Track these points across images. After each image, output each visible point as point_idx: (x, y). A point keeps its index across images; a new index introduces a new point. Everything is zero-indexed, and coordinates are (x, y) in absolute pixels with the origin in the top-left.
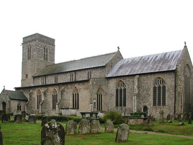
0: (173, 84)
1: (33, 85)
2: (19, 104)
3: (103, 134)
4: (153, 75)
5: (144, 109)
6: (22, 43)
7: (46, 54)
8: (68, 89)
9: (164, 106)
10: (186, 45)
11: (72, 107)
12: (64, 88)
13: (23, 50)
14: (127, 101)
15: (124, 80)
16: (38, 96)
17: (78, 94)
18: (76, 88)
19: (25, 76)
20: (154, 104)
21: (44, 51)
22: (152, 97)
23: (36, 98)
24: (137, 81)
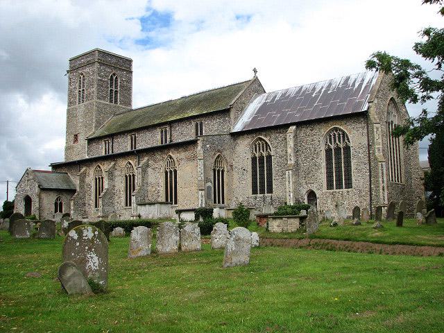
2: (57, 199)
7: (114, 90)
8: (155, 161)
9: (349, 190)
11: (164, 200)
12: (148, 160)
15: (266, 136)
17: (175, 171)
19: (72, 138)
20: (330, 186)
21: (111, 86)
22: (324, 170)
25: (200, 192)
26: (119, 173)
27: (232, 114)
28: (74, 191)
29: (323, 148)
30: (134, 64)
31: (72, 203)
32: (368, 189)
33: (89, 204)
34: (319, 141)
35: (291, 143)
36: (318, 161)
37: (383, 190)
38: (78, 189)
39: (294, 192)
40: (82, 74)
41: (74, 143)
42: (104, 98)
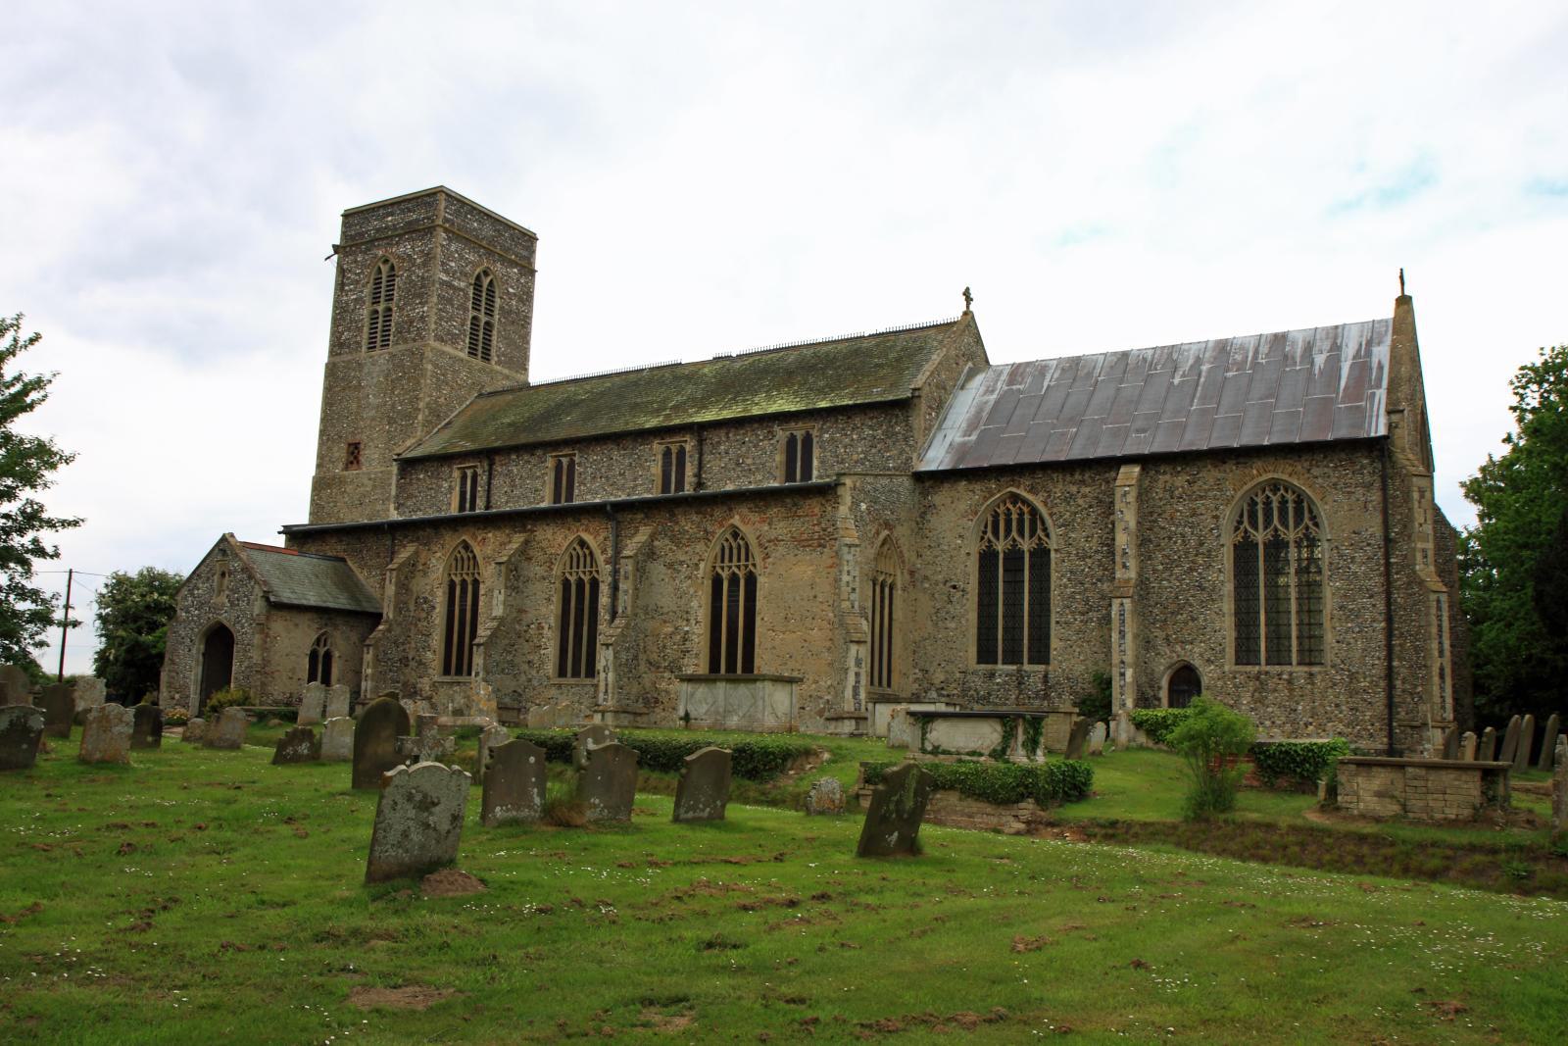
0: (1374, 527)
1: (394, 516)
2: (318, 641)
3: (741, 831)
4: (1230, 466)
5: (1171, 683)
6: (338, 242)
7: (483, 318)
8: (675, 540)
9: (1315, 669)
10: (1406, 293)
11: (702, 667)
12: (653, 537)
13: (340, 286)
14: (1055, 631)
15: (1032, 490)
16: (452, 586)
17: (751, 580)
18: (736, 535)
19: (340, 452)
20: (1245, 652)
21: (476, 307)
22: (1228, 606)
23: (440, 599)
24: (1131, 498)
25: (854, 648)
26: (540, 571)
27: (918, 420)
28: (376, 618)
29: (1228, 540)
30: (540, 247)
31: (368, 657)
32: (1379, 671)
33: (420, 663)
34: (1216, 517)
35: (1127, 516)
36: (1212, 576)
37: (1442, 676)
38: (389, 612)
39: (1136, 665)
40: (386, 261)
41: (346, 468)
42: (454, 340)
